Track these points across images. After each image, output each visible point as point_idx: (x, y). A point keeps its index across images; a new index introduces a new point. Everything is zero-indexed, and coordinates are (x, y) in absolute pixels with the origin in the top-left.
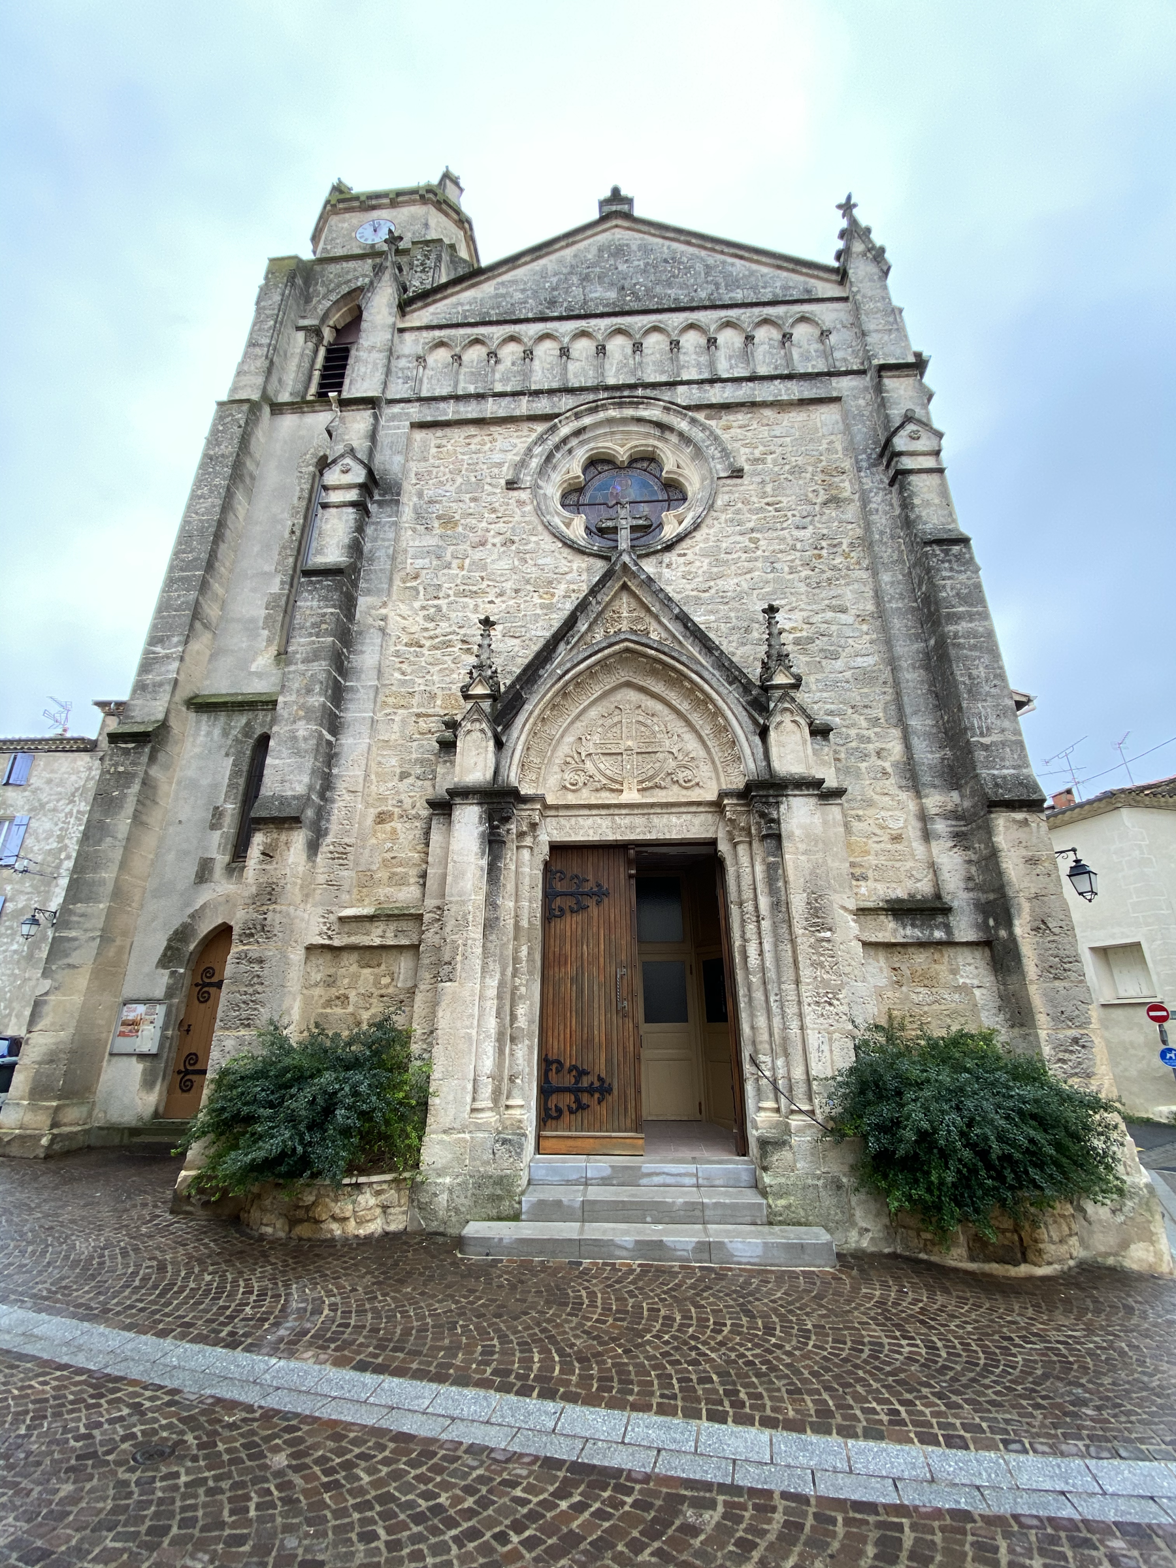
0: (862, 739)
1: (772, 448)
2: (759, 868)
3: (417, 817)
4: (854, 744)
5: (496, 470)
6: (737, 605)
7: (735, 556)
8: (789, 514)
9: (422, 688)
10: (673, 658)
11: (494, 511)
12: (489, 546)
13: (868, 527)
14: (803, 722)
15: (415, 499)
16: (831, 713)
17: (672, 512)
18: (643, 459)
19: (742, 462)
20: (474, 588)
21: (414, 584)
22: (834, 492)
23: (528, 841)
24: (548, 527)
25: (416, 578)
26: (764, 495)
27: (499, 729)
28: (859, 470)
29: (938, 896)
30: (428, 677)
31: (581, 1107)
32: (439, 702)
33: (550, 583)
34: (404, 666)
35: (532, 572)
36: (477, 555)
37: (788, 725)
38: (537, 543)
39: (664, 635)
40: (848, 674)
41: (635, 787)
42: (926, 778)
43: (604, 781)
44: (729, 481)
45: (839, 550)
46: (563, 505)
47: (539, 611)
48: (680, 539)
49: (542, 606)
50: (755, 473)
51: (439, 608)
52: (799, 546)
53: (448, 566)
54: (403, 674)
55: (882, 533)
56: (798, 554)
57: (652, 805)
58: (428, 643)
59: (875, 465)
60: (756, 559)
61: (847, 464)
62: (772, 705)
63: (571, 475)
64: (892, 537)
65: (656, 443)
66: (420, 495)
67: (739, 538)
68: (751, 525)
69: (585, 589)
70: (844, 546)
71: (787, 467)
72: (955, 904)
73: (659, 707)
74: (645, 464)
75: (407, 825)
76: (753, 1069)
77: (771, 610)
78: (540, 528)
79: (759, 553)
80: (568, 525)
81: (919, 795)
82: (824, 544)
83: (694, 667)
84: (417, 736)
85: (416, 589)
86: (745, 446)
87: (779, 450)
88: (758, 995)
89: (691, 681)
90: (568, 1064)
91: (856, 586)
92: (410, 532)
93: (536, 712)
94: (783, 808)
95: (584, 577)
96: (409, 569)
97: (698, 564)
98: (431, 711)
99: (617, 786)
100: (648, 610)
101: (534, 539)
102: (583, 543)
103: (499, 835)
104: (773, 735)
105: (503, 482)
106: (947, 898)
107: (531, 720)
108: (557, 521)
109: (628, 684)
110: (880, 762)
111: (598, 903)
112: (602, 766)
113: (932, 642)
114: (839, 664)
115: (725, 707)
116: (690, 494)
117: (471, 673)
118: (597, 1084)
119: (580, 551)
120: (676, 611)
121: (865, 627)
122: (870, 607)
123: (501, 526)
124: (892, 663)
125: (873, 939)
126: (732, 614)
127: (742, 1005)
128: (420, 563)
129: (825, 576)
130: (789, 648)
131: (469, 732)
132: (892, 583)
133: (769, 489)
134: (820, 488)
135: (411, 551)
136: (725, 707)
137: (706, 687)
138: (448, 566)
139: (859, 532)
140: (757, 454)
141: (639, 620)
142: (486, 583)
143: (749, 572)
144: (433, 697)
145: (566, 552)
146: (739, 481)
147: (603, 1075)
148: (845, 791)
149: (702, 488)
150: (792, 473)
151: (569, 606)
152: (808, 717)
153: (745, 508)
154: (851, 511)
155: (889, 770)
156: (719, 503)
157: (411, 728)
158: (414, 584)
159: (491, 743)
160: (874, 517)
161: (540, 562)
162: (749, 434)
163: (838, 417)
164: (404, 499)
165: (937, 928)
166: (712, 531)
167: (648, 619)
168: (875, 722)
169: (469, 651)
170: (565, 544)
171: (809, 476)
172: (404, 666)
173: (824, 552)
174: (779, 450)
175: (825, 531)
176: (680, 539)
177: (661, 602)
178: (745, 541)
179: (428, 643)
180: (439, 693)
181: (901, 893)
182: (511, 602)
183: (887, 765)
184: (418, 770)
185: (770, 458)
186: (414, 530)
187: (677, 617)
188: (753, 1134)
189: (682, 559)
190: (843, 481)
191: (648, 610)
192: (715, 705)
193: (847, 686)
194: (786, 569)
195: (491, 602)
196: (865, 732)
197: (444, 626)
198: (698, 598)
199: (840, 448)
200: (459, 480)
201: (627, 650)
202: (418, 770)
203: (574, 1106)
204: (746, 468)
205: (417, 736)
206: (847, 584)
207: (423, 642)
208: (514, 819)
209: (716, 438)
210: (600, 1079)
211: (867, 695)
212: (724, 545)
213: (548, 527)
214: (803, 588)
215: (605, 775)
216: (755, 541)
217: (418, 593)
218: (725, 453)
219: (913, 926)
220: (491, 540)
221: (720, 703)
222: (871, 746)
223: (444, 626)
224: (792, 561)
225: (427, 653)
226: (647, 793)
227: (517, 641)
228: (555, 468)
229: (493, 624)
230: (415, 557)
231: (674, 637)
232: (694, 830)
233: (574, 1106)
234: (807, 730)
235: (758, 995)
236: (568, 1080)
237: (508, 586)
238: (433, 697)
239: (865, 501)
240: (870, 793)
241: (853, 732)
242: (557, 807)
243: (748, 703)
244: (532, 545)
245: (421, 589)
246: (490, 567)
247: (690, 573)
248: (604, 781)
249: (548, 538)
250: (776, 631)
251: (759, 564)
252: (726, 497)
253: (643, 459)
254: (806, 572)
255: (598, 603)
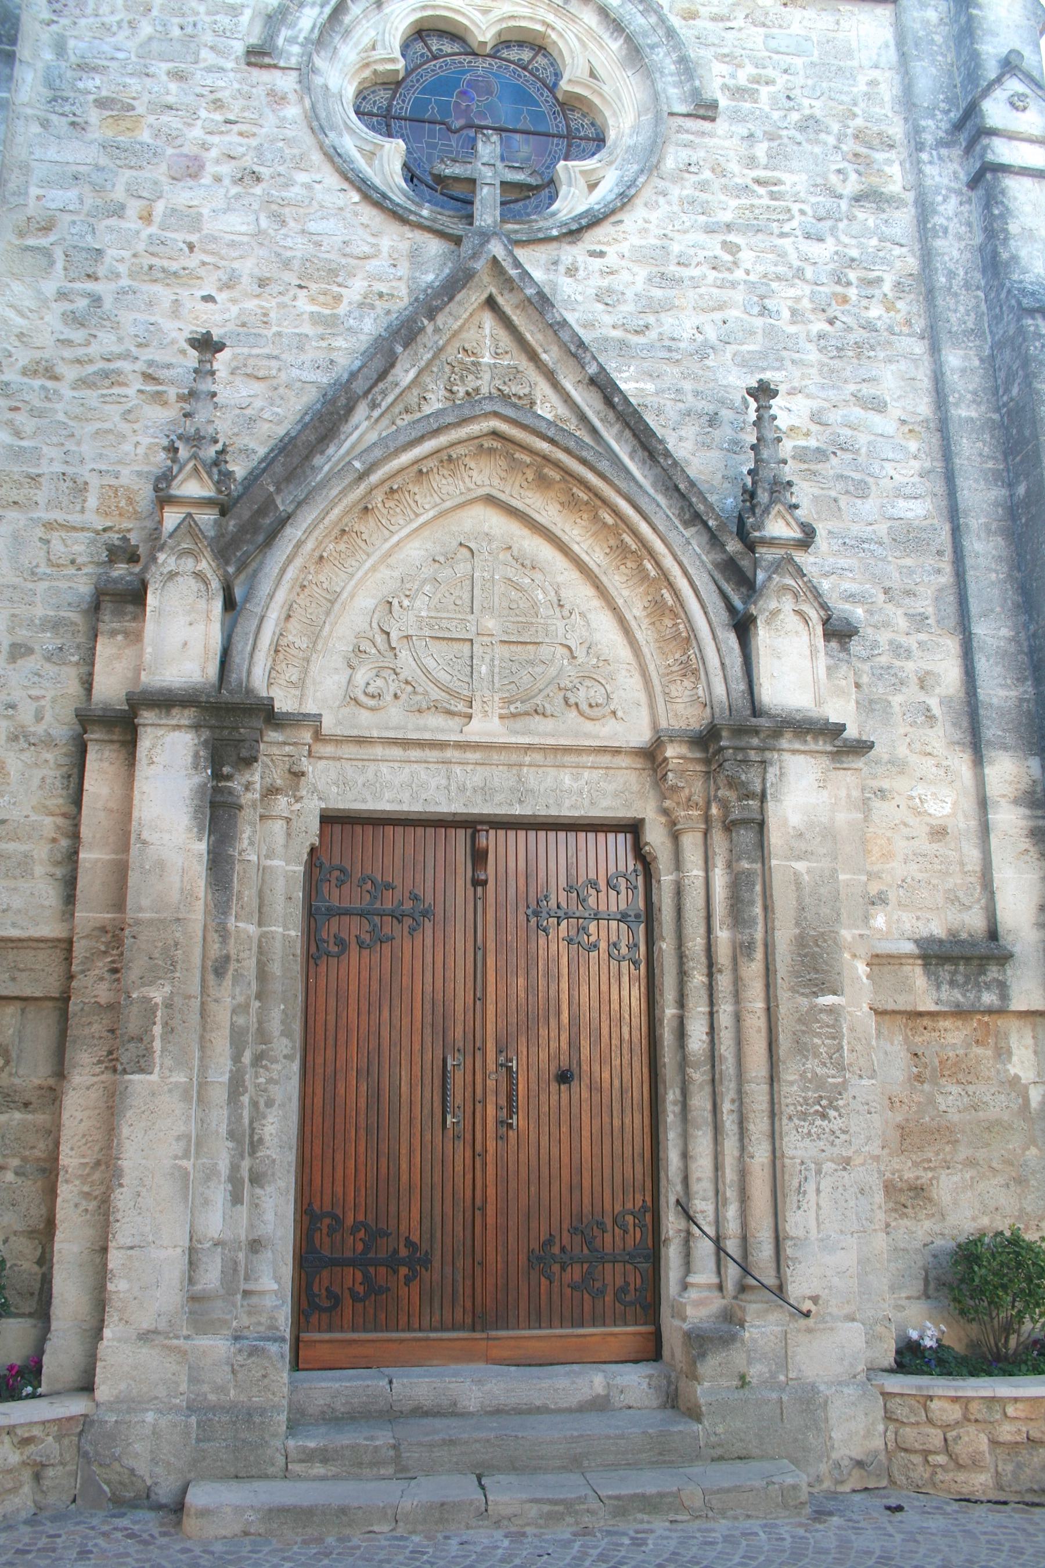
0: (899, 651)
1: (770, 72)
2: (720, 879)
3: (49, 742)
4: (884, 660)
5: (224, 20)
6: (696, 368)
7: (695, 272)
8: (795, 207)
9: (58, 468)
10: (584, 462)
11: (218, 104)
12: (207, 179)
13: (927, 257)
14: (814, 615)
15: (48, 55)
16: (850, 597)
17: (576, 165)
18: (521, 44)
19: (714, 90)
20: (174, 266)
21: (43, 242)
22: (875, 180)
23: (282, 803)
24: (334, 157)
25: (47, 228)
26: (751, 162)
27: (231, 570)
28: (920, 147)
29: (993, 934)
30: (70, 445)
31: (373, 1289)
32: (92, 502)
33: (333, 272)
34: (20, 418)
35: (298, 247)
36: (182, 196)
37: (791, 621)
38: (308, 187)
39: (562, 410)
40: (882, 529)
41: (496, 708)
42: (991, 731)
43: (436, 694)
44: (690, 124)
45: (877, 292)
46: (357, 113)
47: (307, 329)
48: (592, 221)
49: (316, 319)
50: (737, 117)
51: (96, 300)
52: (809, 273)
53: (119, 211)
54: (18, 434)
55: (951, 275)
56: (807, 289)
57: (528, 748)
58: (70, 373)
59: (947, 145)
60: (733, 285)
61: (897, 130)
62: (761, 576)
63: (380, 53)
64: (967, 286)
65: (550, 18)
66: (60, 48)
67: (702, 238)
68: (727, 217)
69: (402, 301)
70: (887, 287)
71: (795, 116)
72: (1017, 949)
73: (546, 552)
74: (526, 55)
75: (26, 756)
76: (682, 1224)
77: (763, 392)
78: (316, 157)
79: (739, 274)
80: (370, 156)
81: (978, 761)
82: (852, 276)
83: (623, 485)
84: (43, 569)
85: (46, 253)
86: (723, 58)
87: (781, 80)
88: (701, 1102)
89: (616, 512)
90: (350, 1221)
91: (903, 365)
92: (35, 129)
93: (310, 545)
94: (772, 772)
95: (403, 270)
96: (32, 208)
97: (625, 276)
98: (75, 519)
99: (461, 707)
100: (533, 356)
101: (302, 177)
102: (400, 199)
103: (230, 792)
104: (763, 636)
105: (239, 48)
106: (1007, 940)
107: (298, 562)
108: (348, 145)
109: (490, 500)
110: (922, 697)
111: (412, 930)
112: (430, 663)
113: (1021, 490)
114: (868, 507)
115: (676, 572)
116: (612, 135)
117: (172, 450)
118: (403, 1252)
119: (398, 215)
120: (592, 369)
121: (913, 446)
122: (924, 407)
123: (231, 139)
124: (954, 514)
125: (891, 1006)
126: (688, 386)
127: (670, 1118)
128: (59, 197)
129: (852, 338)
130: (788, 472)
131: (172, 575)
132: (963, 371)
133: (761, 150)
134: (850, 168)
135: (39, 171)
136: (676, 572)
137: (644, 528)
138: (119, 211)
139: (913, 263)
140: (742, 79)
141: (516, 373)
142: (199, 256)
143: (720, 308)
144: (80, 489)
145: (369, 214)
146: (707, 125)
147: (415, 1238)
148: (871, 746)
149: (636, 129)
150: (802, 128)
151: (370, 327)
152: (824, 606)
153: (717, 184)
154: (903, 220)
155: (936, 711)
156: (670, 163)
157: (33, 554)
158: (43, 242)
159: (218, 605)
160: (939, 243)
161: (312, 227)
162: (730, 35)
163: (887, 34)
164: (24, 51)
165: (988, 987)
166: (654, 216)
167: (532, 373)
168: (919, 621)
169: (158, 398)
170: (366, 197)
171: (831, 140)
172: (20, 418)
173: (852, 292)
174: (781, 80)
175: (854, 253)
176: (592, 221)
177: (563, 346)
178: (713, 246)
179: (70, 373)
180: (94, 481)
181: (937, 929)
182: (251, 304)
183: (933, 702)
184: (48, 641)
185: (764, 91)
186: (45, 124)
187: (592, 381)
188: (672, 1329)
189: (597, 263)
190: (889, 162)
191: (533, 356)
192: (658, 564)
193: (879, 551)
194: (786, 314)
195: (208, 299)
196: (903, 640)
197: (106, 342)
198: (623, 344)
199: (887, 98)
200: (146, 29)
201: (495, 434)
202: (48, 641)
203: (360, 1289)
204: (723, 102)
205: (43, 569)
206: (889, 360)
207: (61, 369)
208: (258, 767)
209: (671, 33)
210: (409, 1243)
211: (910, 570)
212: (676, 248)
213: (334, 157)
214: (812, 355)
215: (436, 682)
216: (732, 248)
217: (52, 263)
218: (687, 67)
219: (952, 983)
220: (211, 169)
221: (669, 562)
222: (910, 666)
223: (106, 342)
224: (797, 299)
225: (68, 393)
226: (519, 724)
227: (257, 387)
228: (347, 33)
229: (220, 347)
230: (46, 183)
231: (583, 418)
232: (605, 803)
233: (360, 1289)
234: (819, 630)
235: (701, 1102)
236: (352, 1246)
237: (247, 268)
238: (80, 489)
239: (924, 210)
240: (902, 751)
241: (884, 637)
242: (339, 741)
243: (717, 565)
244: (296, 189)
245: (58, 254)
246: (210, 226)
247: (610, 291)
248: (436, 694)
249: (332, 180)
250: (770, 435)
251: (739, 296)
252: (684, 154)
253: (521, 44)
254: (820, 325)
255: (437, 330)
